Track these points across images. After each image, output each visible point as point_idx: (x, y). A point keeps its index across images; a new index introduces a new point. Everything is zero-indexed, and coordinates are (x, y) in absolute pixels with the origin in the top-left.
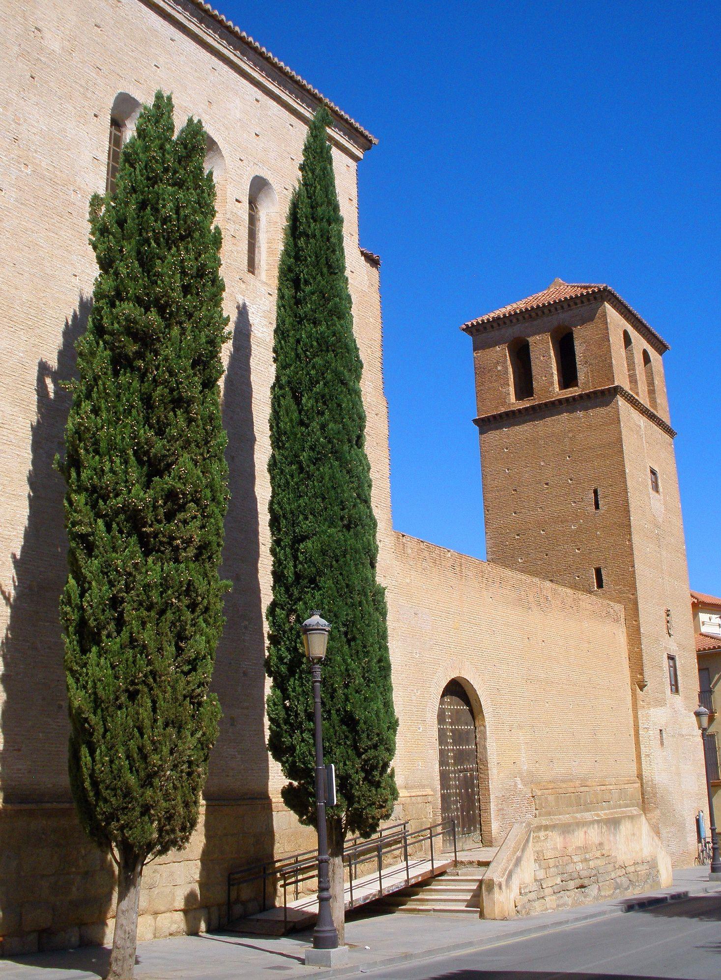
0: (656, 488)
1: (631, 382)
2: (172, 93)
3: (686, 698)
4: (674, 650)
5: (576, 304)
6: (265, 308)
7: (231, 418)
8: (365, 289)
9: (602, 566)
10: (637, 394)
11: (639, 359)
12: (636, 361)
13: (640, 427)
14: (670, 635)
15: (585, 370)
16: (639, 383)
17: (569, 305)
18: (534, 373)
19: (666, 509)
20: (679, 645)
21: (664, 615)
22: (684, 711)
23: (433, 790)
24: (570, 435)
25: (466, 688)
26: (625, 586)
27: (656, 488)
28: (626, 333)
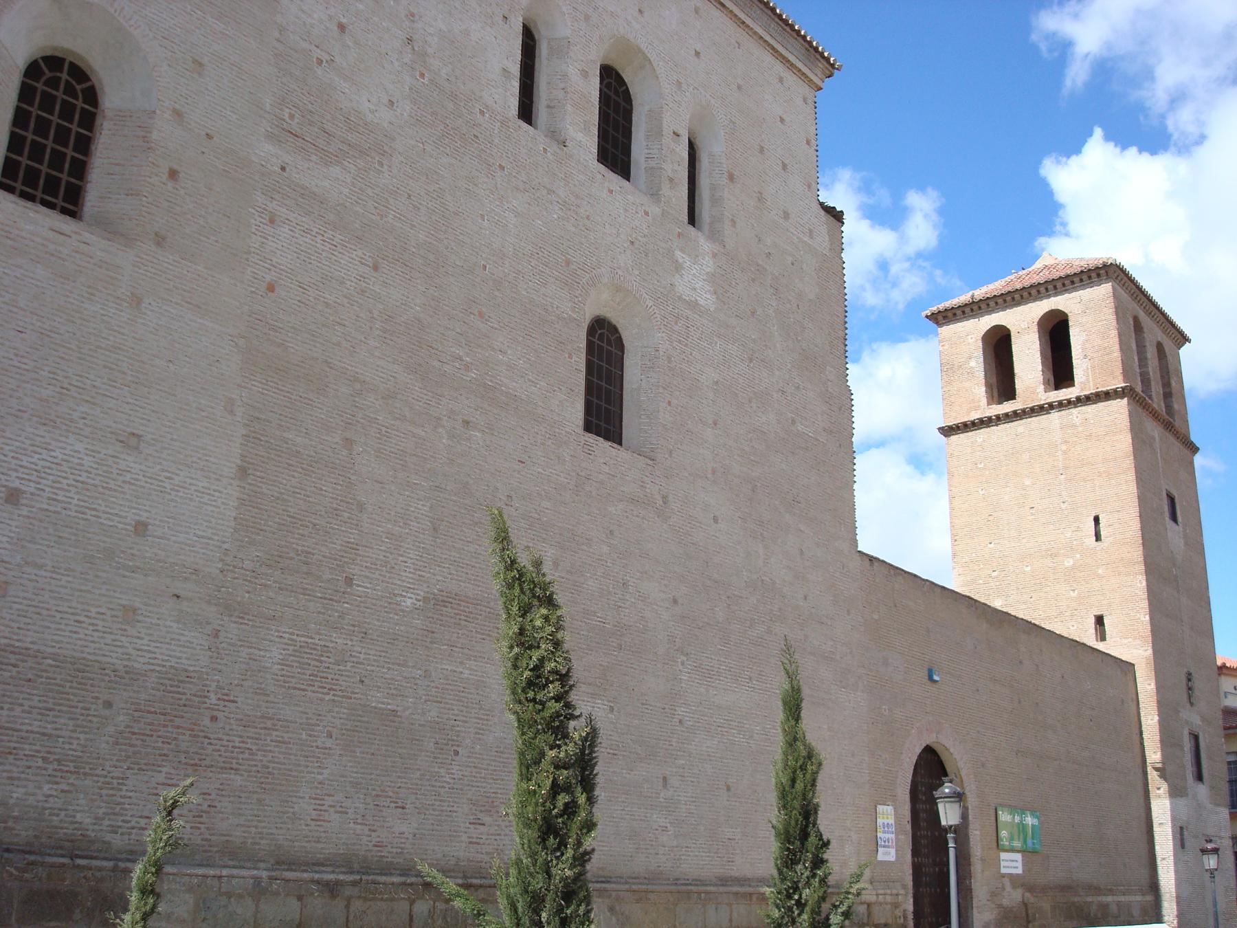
0: (1174, 518)
1: (1142, 381)
2: (107, 227)
3: (1212, 788)
4: (1196, 720)
5: (1073, 283)
6: (708, 270)
7: (669, 403)
8: (826, 252)
9: (1105, 613)
10: (1150, 397)
11: (1151, 353)
12: (1149, 355)
13: (1153, 438)
14: (1192, 704)
15: (1084, 366)
16: (1153, 383)
17: (1064, 285)
18: (1016, 371)
19: (1186, 544)
20: (1203, 719)
21: (1184, 681)
22: (1210, 806)
23: (904, 887)
24: (1064, 448)
25: (943, 758)
26: (1135, 638)
27: (1174, 518)
28: (1136, 319)
